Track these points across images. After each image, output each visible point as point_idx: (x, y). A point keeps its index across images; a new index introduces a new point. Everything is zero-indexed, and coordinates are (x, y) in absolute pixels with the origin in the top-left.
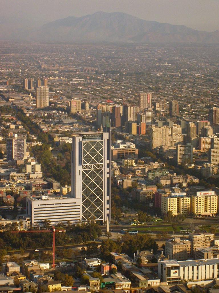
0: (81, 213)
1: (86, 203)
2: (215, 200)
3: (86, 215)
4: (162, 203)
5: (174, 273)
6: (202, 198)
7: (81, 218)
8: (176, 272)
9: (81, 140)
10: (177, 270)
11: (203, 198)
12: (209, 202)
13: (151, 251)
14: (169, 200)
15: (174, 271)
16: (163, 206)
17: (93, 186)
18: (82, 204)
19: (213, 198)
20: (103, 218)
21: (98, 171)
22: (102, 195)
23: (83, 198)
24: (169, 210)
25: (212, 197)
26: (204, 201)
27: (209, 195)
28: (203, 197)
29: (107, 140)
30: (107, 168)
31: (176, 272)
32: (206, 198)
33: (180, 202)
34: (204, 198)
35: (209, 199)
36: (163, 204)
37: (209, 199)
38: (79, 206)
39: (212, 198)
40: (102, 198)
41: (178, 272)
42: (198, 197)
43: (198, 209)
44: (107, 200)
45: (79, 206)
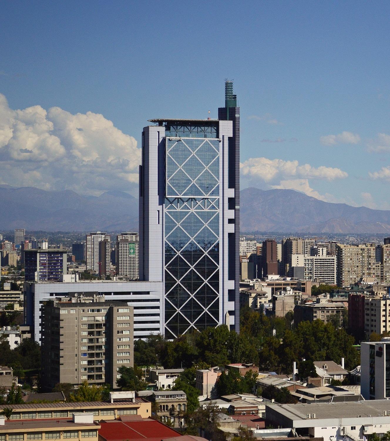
0: (162, 318)
22: (217, 276)
23: (169, 282)
30: (230, 279)
38: (158, 300)
40: (217, 287)
45: (158, 300)
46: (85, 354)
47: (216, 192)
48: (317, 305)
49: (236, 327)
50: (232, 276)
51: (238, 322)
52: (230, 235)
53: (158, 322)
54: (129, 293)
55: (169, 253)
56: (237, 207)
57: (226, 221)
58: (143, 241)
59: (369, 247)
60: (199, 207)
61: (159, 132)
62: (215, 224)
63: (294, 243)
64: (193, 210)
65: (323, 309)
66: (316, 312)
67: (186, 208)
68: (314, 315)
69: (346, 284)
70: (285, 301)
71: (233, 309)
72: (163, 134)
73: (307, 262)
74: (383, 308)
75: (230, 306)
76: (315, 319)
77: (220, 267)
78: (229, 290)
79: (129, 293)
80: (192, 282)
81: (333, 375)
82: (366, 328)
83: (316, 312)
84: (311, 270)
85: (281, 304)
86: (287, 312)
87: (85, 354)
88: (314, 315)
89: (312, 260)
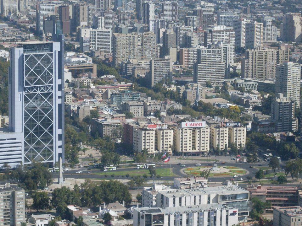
0: (23, 152)
6: (188, 131)
11: (190, 131)
14: (143, 134)
19: (203, 130)
22: (52, 127)
23: (26, 132)
25: (202, 129)
27: (199, 126)
30: (59, 128)
34: (191, 131)
38: (21, 143)
39: (202, 130)
40: (52, 132)
42: (184, 129)
45: (21, 143)
46: (2, 220)
47: (51, 82)
48: (105, 123)
49: (63, 154)
50: (60, 127)
51: (64, 152)
52: (59, 105)
53: (21, 154)
54: (5, 140)
55: (26, 116)
56: (63, 90)
57: (57, 97)
58: (12, 106)
59: (133, 35)
60: (42, 91)
61: (20, 51)
62: (51, 99)
63: (81, 7)
64: (39, 92)
65: (108, 125)
66: (104, 127)
67: (35, 91)
68: (104, 128)
69: (119, 62)
70: (85, 109)
71: (61, 144)
72: (22, 52)
73: (92, 34)
74: (143, 135)
75: (59, 143)
76: (104, 136)
77: (54, 122)
78: (59, 135)
79: (5, 140)
80: (38, 131)
81: (119, 211)
82: (134, 144)
83: (104, 127)
84: (94, 39)
85: (83, 111)
86: (85, 116)
87: (2, 220)
88: (104, 128)
89: (95, 32)
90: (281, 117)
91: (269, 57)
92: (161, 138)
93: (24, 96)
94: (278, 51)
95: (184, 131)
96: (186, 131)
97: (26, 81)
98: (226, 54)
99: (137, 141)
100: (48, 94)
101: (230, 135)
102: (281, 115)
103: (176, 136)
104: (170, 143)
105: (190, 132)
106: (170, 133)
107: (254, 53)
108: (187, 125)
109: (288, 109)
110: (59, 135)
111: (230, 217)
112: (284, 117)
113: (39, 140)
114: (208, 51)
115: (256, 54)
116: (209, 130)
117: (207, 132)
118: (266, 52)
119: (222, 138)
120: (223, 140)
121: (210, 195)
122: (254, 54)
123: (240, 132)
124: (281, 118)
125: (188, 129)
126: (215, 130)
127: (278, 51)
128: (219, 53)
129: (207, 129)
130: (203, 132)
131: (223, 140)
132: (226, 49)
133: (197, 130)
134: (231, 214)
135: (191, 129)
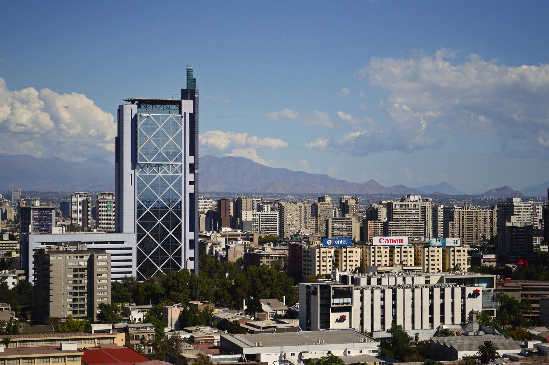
0: (134, 263)
1: (144, 244)
2: (409, 254)
3: (145, 268)
4: (303, 262)
5: (337, 321)
6: (383, 250)
7: (134, 275)
8: (342, 319)
9: (135, 111)
10: (346, 314)
11: (385, 250)
12: (399, 254)
13: (282, 301)
14: (316, 253)
15: (338, 315)
16: (306, 267)
17: (159, 234)
18: (137, 245)
19: (405, 250)
20: (181, 161)
21: (171, 179)
22: (180, 228)
23: (140, 234)
24: (317, 272)
25: (403, 247)
26: (388, 256)
27: (398, 244)
28: (386, 247)
29: (190, 115)
30: (190, 231)
31: (342, 319)
32: (392, 252)
33: (340, 259)
34: (388, 250)
35: (398, 252)
36: (305, 263)
37: (398, 252)
38: (131, 249)
39: (403, 249)
40: (180, 237)
41: (347, 318)
42: (376, 247)
43: (377, 259)
44: (190, 194)
45: (131, 249)
48: (262, 253)
50: (192, 229)
51: (197, 266)
53: (131, 266)
54: (107, 243)
55: (140, 210)
56: (196, 171)
57: (187, 183)
59: (306, 205)
60: (165, 172)
62: (178, 185)
63: (244, 201)
64: (160, 174)
65: (268, 256)
66: (262, 258)
72: (135, 111)
75: (191, 253)
77: (182, 221)
78: (190, 241)
79: (107, 243)
81: (276, 310)
83: (262, 258)
86: (237, 258)
90: (514, 248)
91: (480, 219)
92: (344, 259)
93: (138, 178)
94: (492, 212)
95: (377, 250)
96: (379, 250)
97: (140, 154)
98: (425, 216)
99: (308, 265)
100: (174, 177)
101: (444, 259)
102: (514, 245)
103: (365, 258)
104: (356, 263)
105: (386, 252)
106: (356, 252)
107: (461, 213)
108: (381, 241)
109: (524, 240)
110: (190, 241)
111: (468, 301)
112: (519, 242)
113: (148, 212)
114: (401, 205)
115: (463, 214)
116: (413, 250)
117: (410, 252)
118: (476, 212)
119: (433, 263)
120: (434, 265)
121: (429, 277)
122: (461, 215)
123: (459, 253)
124: (514, 250)
125: (382, 247)
126: (422, 251)
127: (492, 212)
128: (417, 208)
129: (411, 247)
130: (404, 252)
131: (434, 265)
132: (424, 208)
133: (397, 250)
134: (470, 296)
135: (387, 248)
